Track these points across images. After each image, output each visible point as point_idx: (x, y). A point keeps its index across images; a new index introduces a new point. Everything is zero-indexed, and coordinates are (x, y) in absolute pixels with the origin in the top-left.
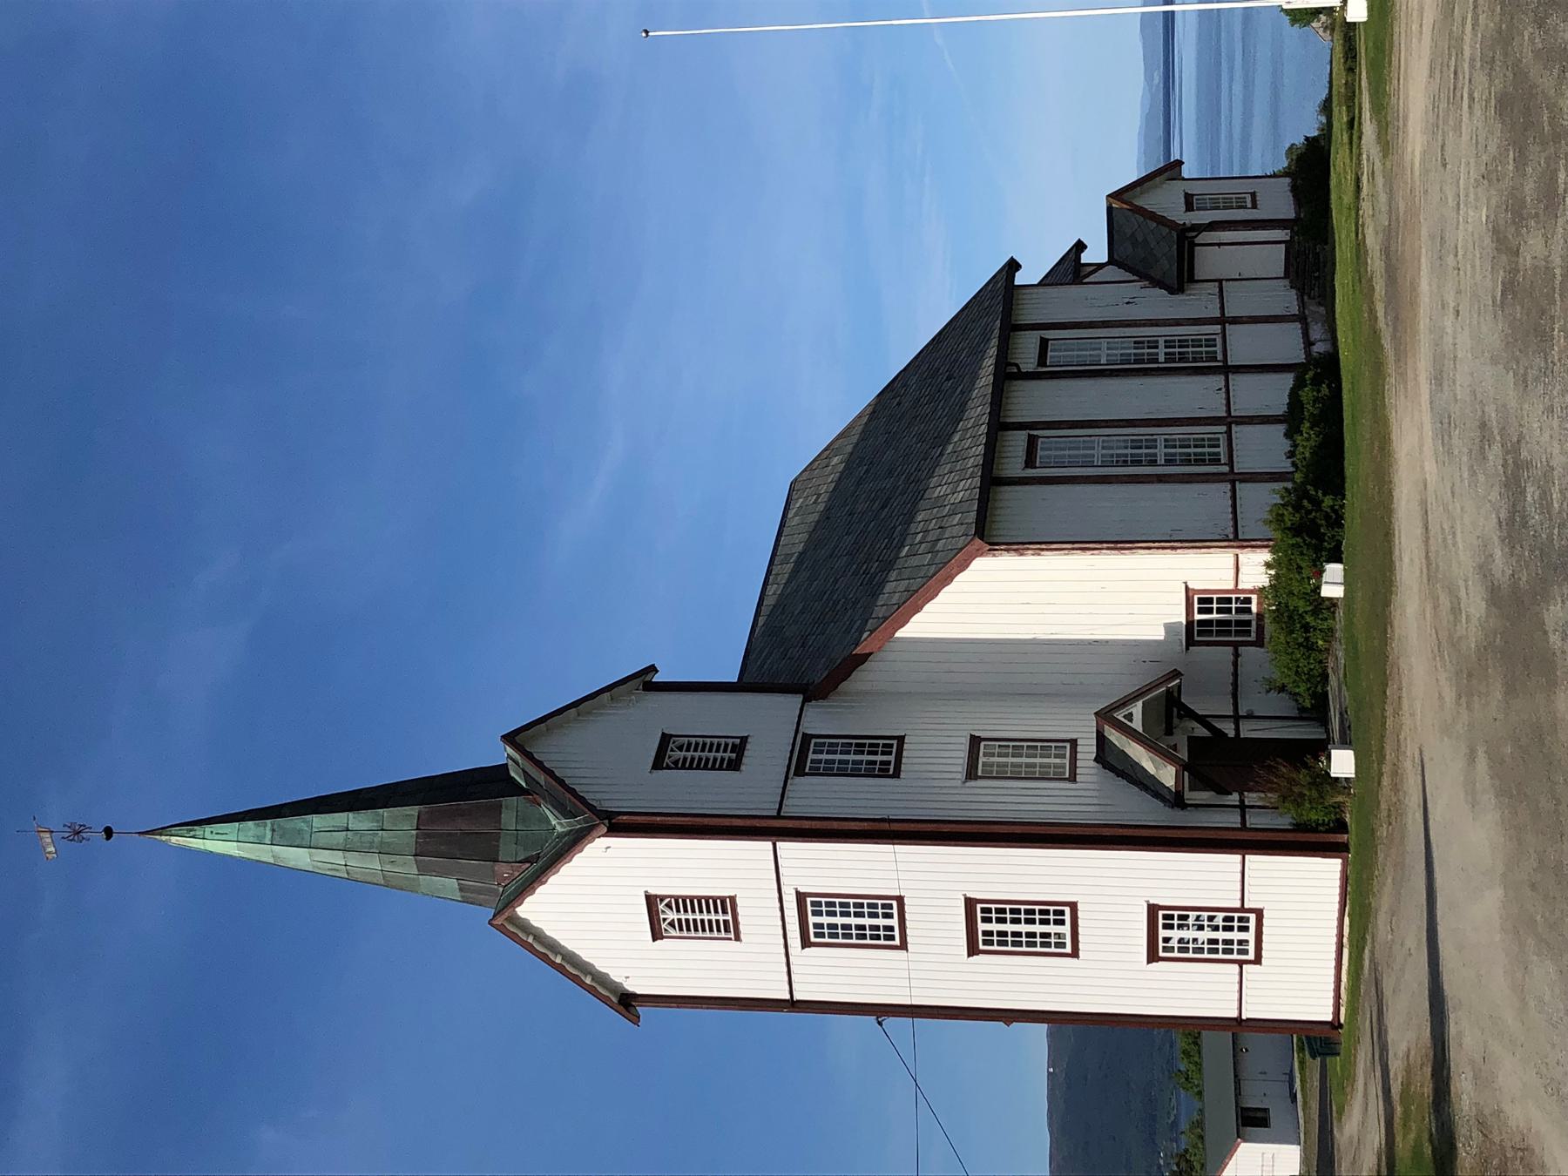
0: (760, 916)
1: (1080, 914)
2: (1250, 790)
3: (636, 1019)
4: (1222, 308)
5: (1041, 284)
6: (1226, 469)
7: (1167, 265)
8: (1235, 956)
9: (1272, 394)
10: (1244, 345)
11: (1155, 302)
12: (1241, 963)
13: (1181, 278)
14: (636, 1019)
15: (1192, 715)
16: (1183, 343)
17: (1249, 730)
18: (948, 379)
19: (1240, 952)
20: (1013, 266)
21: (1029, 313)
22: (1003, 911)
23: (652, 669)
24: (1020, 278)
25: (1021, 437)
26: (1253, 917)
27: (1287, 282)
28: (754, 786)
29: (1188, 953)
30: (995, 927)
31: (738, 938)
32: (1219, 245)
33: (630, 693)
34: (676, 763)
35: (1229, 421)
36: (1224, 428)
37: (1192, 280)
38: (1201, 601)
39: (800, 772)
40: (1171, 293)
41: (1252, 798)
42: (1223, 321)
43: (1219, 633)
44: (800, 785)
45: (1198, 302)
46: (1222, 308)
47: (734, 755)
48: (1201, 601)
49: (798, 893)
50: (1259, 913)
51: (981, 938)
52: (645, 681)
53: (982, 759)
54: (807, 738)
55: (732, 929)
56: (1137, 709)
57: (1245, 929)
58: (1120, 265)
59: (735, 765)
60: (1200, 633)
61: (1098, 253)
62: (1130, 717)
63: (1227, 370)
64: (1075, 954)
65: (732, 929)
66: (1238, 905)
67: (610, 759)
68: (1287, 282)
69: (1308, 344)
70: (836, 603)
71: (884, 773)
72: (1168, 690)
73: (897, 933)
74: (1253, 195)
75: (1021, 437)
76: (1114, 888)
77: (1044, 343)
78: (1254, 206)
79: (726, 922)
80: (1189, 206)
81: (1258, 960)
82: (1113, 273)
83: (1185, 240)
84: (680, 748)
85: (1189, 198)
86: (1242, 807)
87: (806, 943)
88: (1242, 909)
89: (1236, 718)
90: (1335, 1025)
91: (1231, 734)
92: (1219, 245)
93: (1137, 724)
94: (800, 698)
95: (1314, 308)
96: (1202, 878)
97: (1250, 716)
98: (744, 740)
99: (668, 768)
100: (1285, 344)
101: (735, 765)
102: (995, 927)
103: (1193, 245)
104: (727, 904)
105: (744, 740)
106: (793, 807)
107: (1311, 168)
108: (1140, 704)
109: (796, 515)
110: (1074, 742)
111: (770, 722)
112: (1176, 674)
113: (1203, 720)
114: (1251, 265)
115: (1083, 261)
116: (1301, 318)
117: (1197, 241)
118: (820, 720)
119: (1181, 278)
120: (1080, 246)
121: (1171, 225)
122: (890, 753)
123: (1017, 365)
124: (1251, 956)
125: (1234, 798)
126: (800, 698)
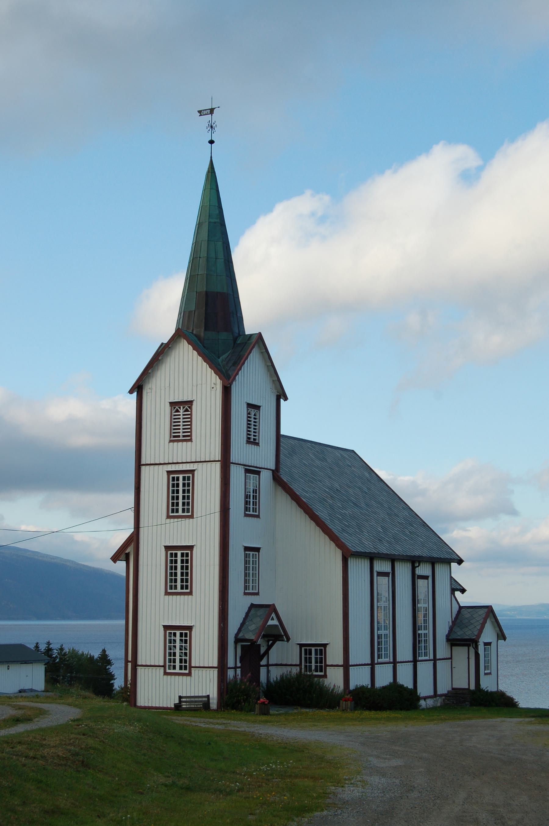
0: (182, 452)
1: (186, 597)
2: (241, 671)
3: (131, 392)
4: (440, 659)
5: (451, 577)
6: (376, 662)
7: (459, 634)
8: (167, 664)
9: (405, 679)
10: (425, 670)
11: (443, 629)
12: (164, 666)
13: (453, 642)
14: (131, 392)
15: (269, 647)
16: (426, 641)
17: (263, 671)
18: (410, 532)
19: (170, 666)
20: (460, 561)
21: (440, 569)
22: (187, 562)
23: (286, 399)
24: (454, 565)
25: (388, 569)
26: (187, 672)
27: (450, 689)
28: (240, 451)
29: (169, 643)
30: (179, 558)
31: (171, 441)
32: (469, 658)
33: (276, 388)
34: (249, 414)
35: (395, 663)
36: (392, 660)
37: (452, 645)
38: (321, 650)
39: (247, 471)
40: (447, 636)
41: (239, 671)
42: (435, 660)
43: (306, 658)
44: (241, 470)
45: (443, 650)
46: (440, 659)
47: (252, 441)
48: (321, 650)
49: (194, 470)
50: (190, 674)
51: (174, 552)
52: (281, 395)
53: (251, 553)
54: (258, 473)
55: (174, 438)
56: (275, 622)
57: (181, 668)
58: (459, 612)
59: (249, 441)
60: (306, 650)
61: (463, 599)
62: (273, 619)
63: (415, 661)
64: (167, 593)
65: (174, 438)
66: (193, 665)
67: (250, 383)
68: (450, 689)
69: (425, 698)
70: (312, 482)
71: (246, 509)
72: (283, 636)
73: (175, 514)
74: (490, 674)
75: (388, 569)
76: (199, 611)
77: (426, 578)
78: (486, 674)
79: (179, 436)
80: (486, 644)
81: (166, 673)
82: (456, 608)
83: (471, 643)
84: (255, 415)
85: (489, 644)
86: (235, 668)
87: (169, 473)
88: (191, 667)
89: (268, 665)
90: (135, 705)
91: (262, 663)
92: (469, 658)
93: (270, 622)
94: (274, 468)
95: (439, 702)
96: (205, 648)
97: (268, 671)
98: (258, 444)
99: (248, 410)
100: (425, 688)
101: (249, 441)
102: (179, 558)
103: (469, 646)
104: (188, 438)
105: (258, 444)
106: (233, 468)
107: (502, 703)
108: (278, 623)
109: (341, 455)
110: (257, 594)
111: (264, 456)
112: (288, 639)
113: (267, 652)
114: (456, 674)
115: (456, 592)
116: (435, 695)
117: (471, 648)
118: (266, 477)
119: (453, 642)
120: (463, 591)
121: (479, 636)
122: (253, 511)
123: (418, 566)
124: (168, 671)
125: (239, 665)
126: (274, 468)
